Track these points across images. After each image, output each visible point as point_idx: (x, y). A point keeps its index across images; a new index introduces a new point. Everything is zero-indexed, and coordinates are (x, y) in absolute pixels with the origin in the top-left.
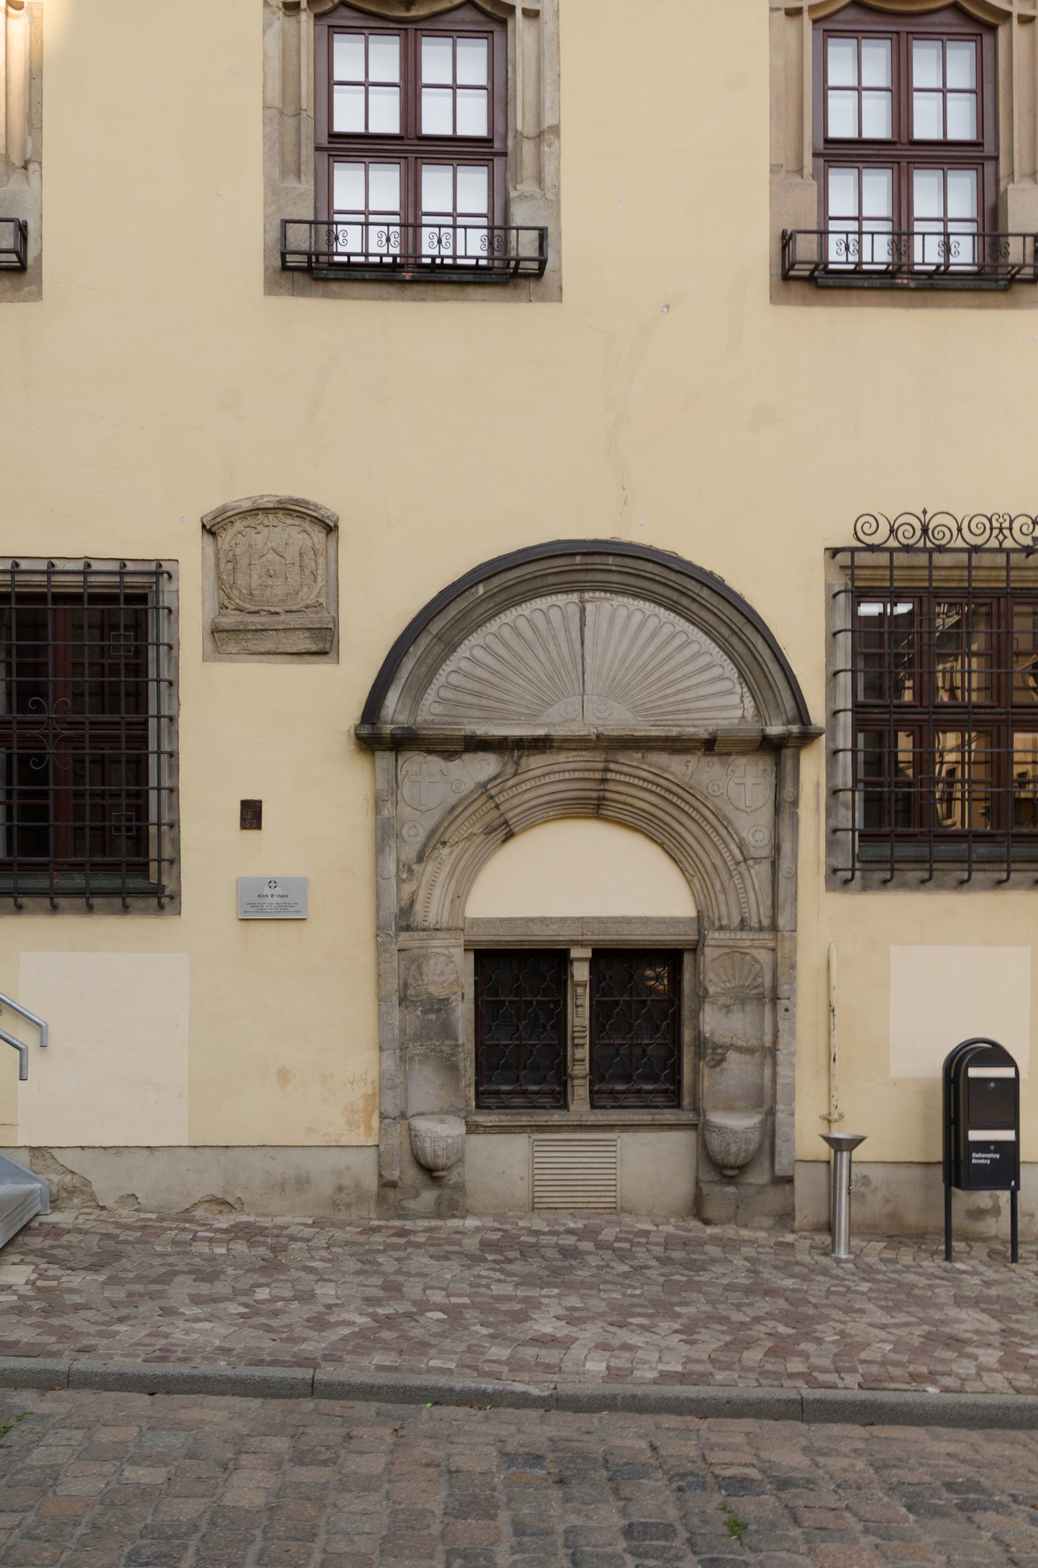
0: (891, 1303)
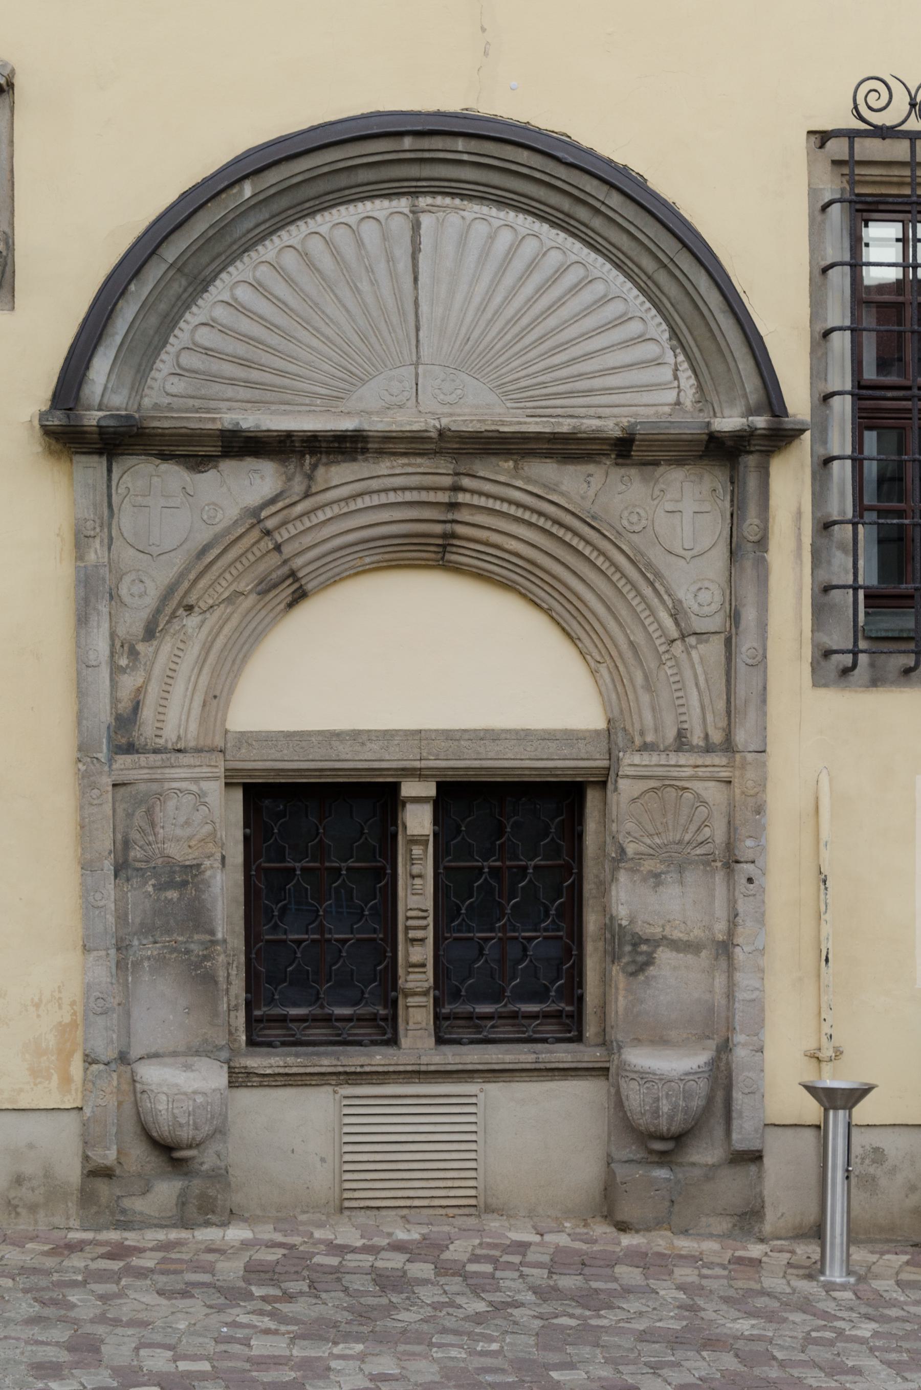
0: (905, 1357)
